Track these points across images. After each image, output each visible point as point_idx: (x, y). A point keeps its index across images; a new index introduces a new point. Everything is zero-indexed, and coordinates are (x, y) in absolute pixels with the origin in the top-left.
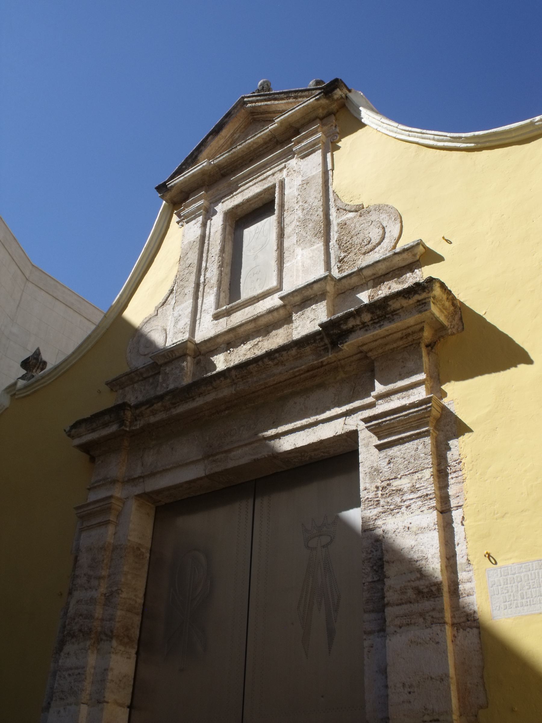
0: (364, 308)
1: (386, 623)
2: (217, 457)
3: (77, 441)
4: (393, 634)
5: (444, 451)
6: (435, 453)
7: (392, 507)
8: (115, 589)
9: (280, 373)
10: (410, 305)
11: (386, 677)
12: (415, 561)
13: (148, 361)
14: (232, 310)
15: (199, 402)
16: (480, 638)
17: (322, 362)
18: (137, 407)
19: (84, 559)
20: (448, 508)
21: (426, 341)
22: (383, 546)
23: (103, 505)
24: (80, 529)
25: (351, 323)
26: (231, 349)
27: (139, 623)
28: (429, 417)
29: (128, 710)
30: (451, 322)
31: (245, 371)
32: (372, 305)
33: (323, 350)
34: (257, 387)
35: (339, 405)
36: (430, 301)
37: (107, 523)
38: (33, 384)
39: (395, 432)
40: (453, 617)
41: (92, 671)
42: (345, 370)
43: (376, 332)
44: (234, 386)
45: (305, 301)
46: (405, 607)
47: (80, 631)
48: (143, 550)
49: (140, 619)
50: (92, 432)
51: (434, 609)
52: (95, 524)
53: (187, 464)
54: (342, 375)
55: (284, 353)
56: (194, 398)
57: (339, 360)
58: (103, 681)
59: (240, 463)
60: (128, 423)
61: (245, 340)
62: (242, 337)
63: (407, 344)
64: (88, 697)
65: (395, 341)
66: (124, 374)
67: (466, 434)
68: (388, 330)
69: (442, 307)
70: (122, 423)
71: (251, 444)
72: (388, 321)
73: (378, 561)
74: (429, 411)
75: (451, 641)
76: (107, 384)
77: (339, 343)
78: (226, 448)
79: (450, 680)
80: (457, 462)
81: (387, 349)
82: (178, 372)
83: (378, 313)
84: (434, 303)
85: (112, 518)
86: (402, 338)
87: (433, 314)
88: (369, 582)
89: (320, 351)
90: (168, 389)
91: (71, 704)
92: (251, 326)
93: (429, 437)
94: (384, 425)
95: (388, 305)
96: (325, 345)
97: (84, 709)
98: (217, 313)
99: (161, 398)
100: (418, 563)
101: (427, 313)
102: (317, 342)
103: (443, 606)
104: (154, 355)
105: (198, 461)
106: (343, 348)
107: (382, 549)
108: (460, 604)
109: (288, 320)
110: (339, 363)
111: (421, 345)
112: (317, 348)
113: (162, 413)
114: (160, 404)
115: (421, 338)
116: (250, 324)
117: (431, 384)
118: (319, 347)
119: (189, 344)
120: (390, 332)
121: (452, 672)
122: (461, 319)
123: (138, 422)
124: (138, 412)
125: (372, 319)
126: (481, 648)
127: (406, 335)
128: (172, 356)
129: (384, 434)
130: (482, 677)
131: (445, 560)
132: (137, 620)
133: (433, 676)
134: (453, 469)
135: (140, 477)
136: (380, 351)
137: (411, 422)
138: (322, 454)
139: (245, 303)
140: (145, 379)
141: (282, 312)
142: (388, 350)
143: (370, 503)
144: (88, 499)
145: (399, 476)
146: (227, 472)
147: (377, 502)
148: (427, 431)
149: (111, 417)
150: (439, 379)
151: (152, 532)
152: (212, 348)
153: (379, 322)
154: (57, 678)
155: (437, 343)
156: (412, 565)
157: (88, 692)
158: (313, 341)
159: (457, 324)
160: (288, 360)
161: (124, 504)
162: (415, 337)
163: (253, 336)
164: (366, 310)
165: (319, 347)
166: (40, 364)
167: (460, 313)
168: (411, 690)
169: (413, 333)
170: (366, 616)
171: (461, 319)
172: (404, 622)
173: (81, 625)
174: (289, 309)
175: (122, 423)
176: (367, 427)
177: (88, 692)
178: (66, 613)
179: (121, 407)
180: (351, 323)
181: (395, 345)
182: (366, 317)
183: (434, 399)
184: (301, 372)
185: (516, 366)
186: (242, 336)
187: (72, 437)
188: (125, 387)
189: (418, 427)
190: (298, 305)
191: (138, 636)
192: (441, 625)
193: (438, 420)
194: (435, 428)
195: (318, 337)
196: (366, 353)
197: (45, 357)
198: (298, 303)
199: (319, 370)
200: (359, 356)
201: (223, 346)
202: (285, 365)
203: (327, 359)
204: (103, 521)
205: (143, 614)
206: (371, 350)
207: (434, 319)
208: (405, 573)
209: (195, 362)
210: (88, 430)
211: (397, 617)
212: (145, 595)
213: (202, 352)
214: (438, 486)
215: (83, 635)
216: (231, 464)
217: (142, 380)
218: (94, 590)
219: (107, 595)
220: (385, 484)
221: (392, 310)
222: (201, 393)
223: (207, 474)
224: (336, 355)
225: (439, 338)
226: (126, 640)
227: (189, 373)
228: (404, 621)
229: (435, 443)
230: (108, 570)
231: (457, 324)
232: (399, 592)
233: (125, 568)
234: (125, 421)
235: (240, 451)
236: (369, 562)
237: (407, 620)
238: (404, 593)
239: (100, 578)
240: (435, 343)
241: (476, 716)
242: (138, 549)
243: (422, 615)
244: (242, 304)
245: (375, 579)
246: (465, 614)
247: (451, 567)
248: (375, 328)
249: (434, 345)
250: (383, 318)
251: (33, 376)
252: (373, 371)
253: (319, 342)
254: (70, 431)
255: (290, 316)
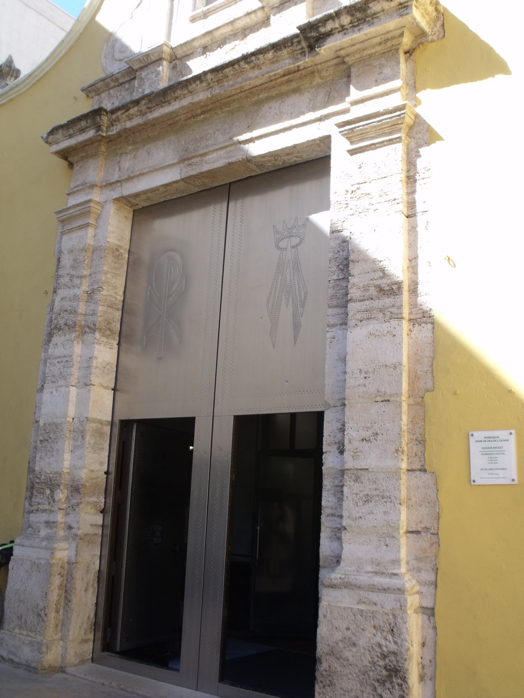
0: (344, 10)
1: (348, 317)
2: (193, 160)
3: (55, 148)
4: (354, 327)
5: (414, 158)
6: (406, 160)
7: (360, 210)
8: (95, 287)
9: (256, 77)
10: (392, 8)
11: (345, 364)
12: (378, 261)
13: (124, 66)
14: (209, 12)
15: (175, 106)
16: (433, 333)
17: (298, 66)
18: (113, 112)
19: (66, 260)
20: (414, 213)
21: (405, 47)
22: (350, 246)
23: (82, 209)
24: (61, 232)
25: (330, 25)
26: (208, 53)
27: (120, 318)
28: (402, 123)
29: (113, 391)
30: (432, 28)
31: (221, 75)
32: (352, 7)
33: (300, 53)
34: (233, 91)
35: (313, 109)
36: (412, 4)
37: (86, 226)
38: (7, 92)
39: (368, 138)
40: (411, 313)
41: (79, 359)
42: (322, 75)
43: (355, 36)
44: (210, 90)
45: (284, 3)
46: (367, 302)
47: (66, 324)
48: (122, 251)
49: (121, 314)
50: (69, 138)
51: (393, 306)
52: (76, 227)
53: (164, 168)
54: (317, 80)
55: (261, 56)
56: (170, 102)
57: (316, 65)
58: (89, 367)
59: (215, 167)
60: (104, 128)
61: (222, 42)
62: (218, 41)
63: (385, 49)
64: (76, 381)
65: (373, 47)
66: (99, 79)
67: (437, 142)
68: (367, 34)
69: (425, 11)
70: (99, 128)
71: (226, 148)
72: (368, 25)
73: (344, 261)
74: (402, 118)
75: (407, 334)
76: (83, 90)
77: (316, 46)
78: (201, 152)
79: (403, 367)
80: (426, 169)
81: (365, 54)
82: (153, 77)
83: (358, 16)
84: (416, 7)
85: (91, 221)
86: (380, 43)
87: (414, 19)
88: (334, 280)
89: (297, 55)
90: (144, 94)
91: (61, 386)
92: (228, 29)
93: (401, 144)
94: (358, 131)
95: (368, 7)
96: (303, 48)
97: (73, 391)
98: (193, 16)
99: (137, 102)
100: (382, 263)
101: (409, 17)
102: (295, 45)
103: (402, 303)
104: (130, 60)
105: (174, 164)
106: (320, 52)
107: (348, 250)
108: (418, 302)
109: (266, 22)
110: (315, 68)
111: (399, 50)
112: (294, 51)
113: (139, 117)
114: (136, 109)
115: (400, 44)
116: (227, 27)
117: (407, 92)
118: (296, 50)
119: (165, 48)
120: (369, 36)
121: (405, 361)
122: (443, 25)
123: (115, 127)
124: (114, 117)
125: (351, 23)
126: (433, 341)
127: (385, 40)
128: (148, 60)
129: (357, 139)
130: (432, 366)
131: (408, 261)
132: (118, 315)
133: (388, 364)
134: (422, 176)
135: (118, 182)
136: (358, 56)
137: (384, 128)
138: (295, 159)
139: (222, 5)
140: (121, 84)
141: (260, 15)
142: (366, 55)
143: (340, 206)
144: (68, 204)
145: (369, 181)
146: (202, 175)
147: (346, 205)
148: (399, 138)
149: (87, 123)
150: (415, 87)
151: (130, 235)
152: (189, 53)
153: (358, 25)
154: (48, 365)
155: (416, 49)
156: (376, 264)
157: (75, 376)
158: (290, 44)
159: (439, 31)
160: (265, 64)
161: (102, 207)
162: (394, 42)
163: (230, 39)
164: (346, 12)
165: (296, 50)
166: (13, 72)
167: (442, 19)
168: (367, 375)
169: (393, 38)
170: (331, 311)
171: (443, 25)
172: (365, 317)
173: (67, 320)
174: (267, 11)
175: (99, 128)
176: (340, 132)
177: (75, 376)
178: (52, 310)
179: (98, 112)
180: (330, 25)
181: (373, 51)
182: (346, 20)
183: (408, 106)
184: (277, 77)
185: (493, 76)
186: (219, 39)
187: (50, 144)
188: (101, 93)
189: (390, 134)
190: (276, 7)
191: (119, 329)
192: (399, 320)
193: (411, 128)
194: (407, 135)
195: (295, 40)
196: (344, 58)
197: (18, 64)
198: (277, 5)
199: (295, 74)
200: (336, 61)
201: (199, 50)
202: (261, 69)
203: (303, 63)
204: (83, 224)
205: (122, 310)
206: (348, 55)
207: (415, 24)
208: (368, 272)
209: (171, 66)
210: (65, 137)
211: (358, 312)
212: (124, 292)
213: (178, 56)
214: (406, 191)
215: (69, 328)
216: (206, 168)
217: (118, 86)
218: (77, 288)
219: (89, 292)
220: (354, 188)
221: (373, 12)
222: (177, 98)
223: (183, 177)
224: (313, 59)
225: (418, 45)
226: (108, 332)
227: (165, 78)
228: (365, 315)
229: (406, 150)
230: (89, 270)
231: (439, 31)
232: (362, 289)
233: (105, 268)
234: (102, 127)
235: (215, 155)
236: (335, 261)
237: (368, 315)
238: (366, 290)
239: (81, 277)
240: (414, 49)
241: (423, 398)
242: (117, 250)
243: (381, 310)
244: (219, 6)
245: (341, 277)
246: (421, 311)
247: (413, 268)
248: (354, 31)
249: (413, 52)
250: (362, 21)
251: (7, 85)
252: (349, 76)
253: (297, 45)
254: (47, 138)
255: (268, 19)
